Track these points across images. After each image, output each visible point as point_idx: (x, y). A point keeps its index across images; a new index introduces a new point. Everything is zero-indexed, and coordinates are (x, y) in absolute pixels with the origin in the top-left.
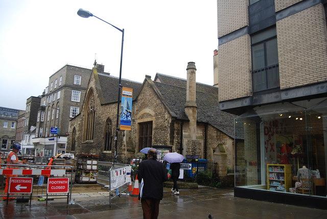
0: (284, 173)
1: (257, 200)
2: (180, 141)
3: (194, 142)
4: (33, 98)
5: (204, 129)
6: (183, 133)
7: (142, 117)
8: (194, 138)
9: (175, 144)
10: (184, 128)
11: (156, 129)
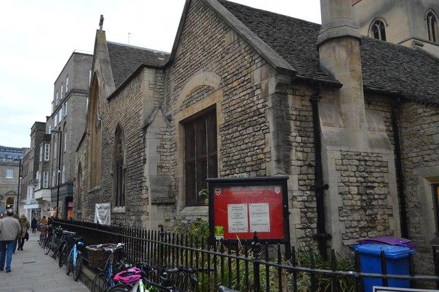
0: (217, 177)
1: (401, 224)
2: (312, 157)
3: (363, 160)
4: (37, 123)
5: (388, 115)
6: (324, 129)
7: (187, 104)
8: (362, 147)
9: (295, 170)
10: (322, 109)
11: (227, 126)
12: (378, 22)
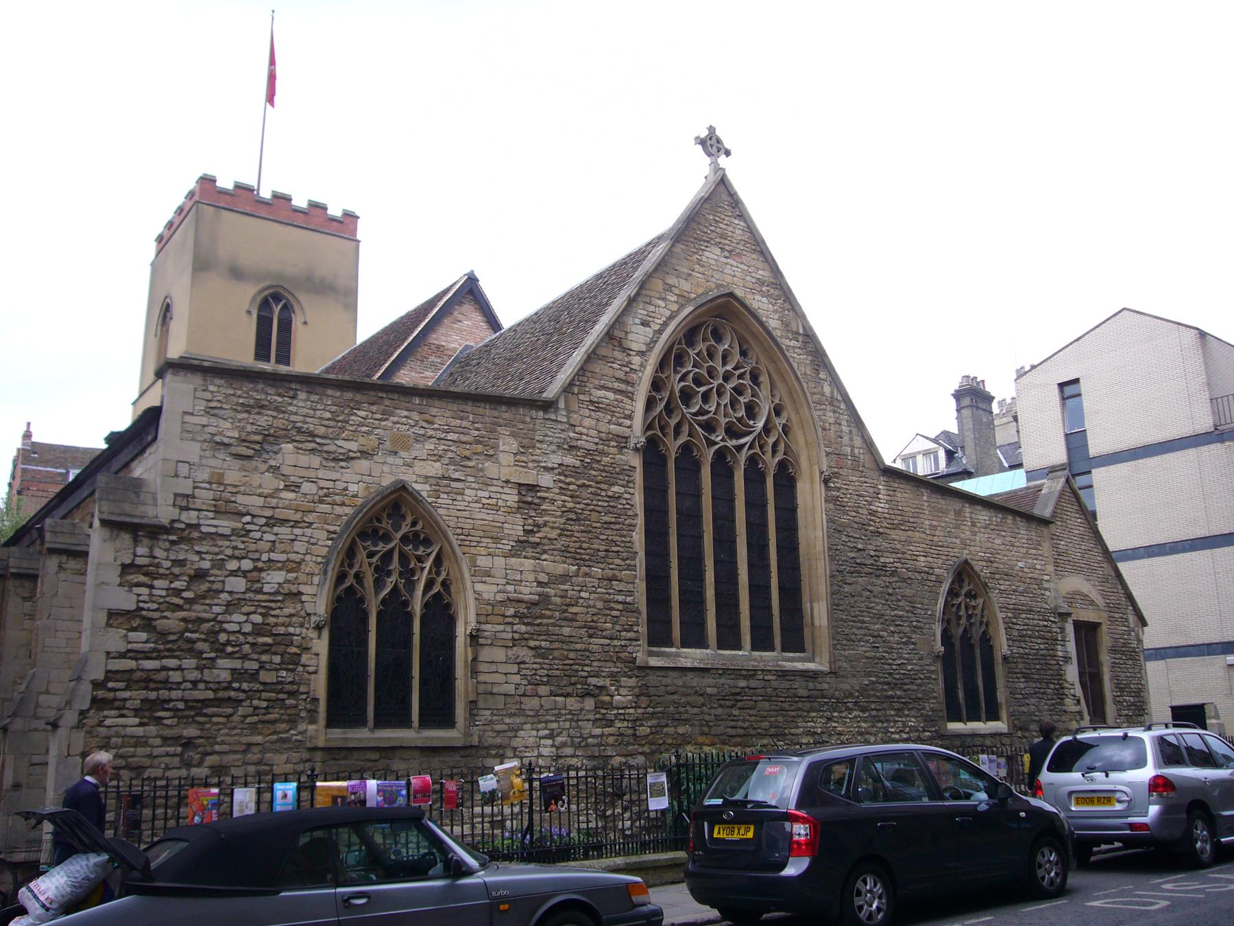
12: (277, 297)
